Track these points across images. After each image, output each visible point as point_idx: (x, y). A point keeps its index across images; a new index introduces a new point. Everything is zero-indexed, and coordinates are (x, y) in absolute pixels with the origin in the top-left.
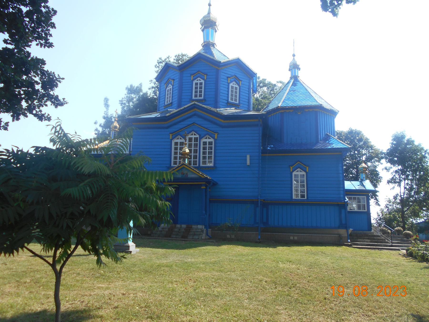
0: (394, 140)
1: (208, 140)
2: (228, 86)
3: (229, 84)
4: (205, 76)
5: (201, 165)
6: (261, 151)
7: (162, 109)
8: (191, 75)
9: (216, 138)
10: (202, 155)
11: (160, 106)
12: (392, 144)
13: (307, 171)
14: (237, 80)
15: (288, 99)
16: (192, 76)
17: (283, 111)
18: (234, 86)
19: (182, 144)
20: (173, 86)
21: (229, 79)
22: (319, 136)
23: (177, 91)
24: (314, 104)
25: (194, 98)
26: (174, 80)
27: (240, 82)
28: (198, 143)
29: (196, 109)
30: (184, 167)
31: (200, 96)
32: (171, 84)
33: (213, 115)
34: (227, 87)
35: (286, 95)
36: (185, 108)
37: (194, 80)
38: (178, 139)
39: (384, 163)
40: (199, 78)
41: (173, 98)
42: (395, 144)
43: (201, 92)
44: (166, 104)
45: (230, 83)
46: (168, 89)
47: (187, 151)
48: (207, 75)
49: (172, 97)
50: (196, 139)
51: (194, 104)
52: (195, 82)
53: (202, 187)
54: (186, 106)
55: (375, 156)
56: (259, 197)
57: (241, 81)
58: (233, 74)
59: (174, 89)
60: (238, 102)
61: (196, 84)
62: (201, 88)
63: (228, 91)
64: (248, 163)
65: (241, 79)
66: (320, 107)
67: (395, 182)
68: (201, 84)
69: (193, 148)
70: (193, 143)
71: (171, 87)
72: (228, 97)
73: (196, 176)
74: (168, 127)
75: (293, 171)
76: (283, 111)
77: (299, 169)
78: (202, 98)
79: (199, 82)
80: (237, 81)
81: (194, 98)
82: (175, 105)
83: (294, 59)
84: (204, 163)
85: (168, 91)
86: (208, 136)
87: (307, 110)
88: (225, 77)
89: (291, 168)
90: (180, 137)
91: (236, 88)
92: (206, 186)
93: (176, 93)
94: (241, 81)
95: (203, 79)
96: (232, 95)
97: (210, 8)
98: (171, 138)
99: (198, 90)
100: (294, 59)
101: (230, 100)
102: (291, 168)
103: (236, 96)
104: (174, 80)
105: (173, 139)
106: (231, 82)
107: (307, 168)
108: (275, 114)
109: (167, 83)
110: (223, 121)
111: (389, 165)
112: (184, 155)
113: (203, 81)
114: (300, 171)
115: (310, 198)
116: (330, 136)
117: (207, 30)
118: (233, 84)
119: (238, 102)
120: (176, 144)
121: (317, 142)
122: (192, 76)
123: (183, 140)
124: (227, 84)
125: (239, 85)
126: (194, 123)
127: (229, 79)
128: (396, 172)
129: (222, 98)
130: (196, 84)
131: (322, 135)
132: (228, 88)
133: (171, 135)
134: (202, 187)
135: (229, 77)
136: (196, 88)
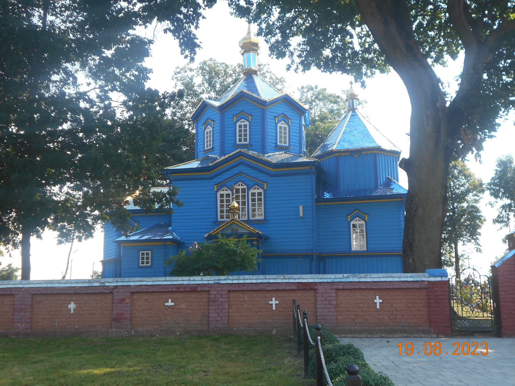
0: (499, 165)
1: (256, 191)
2: (276, 127)
3: (276, 124)
4: (250, 117)
5: (251, 218)
6: (314, 201)
7: (201, 155)
8: (234, 116)
9: (265, 188)
10: (250, 207)
11: (198, 151)
12: (496, 171)
13: (367, 220)
14: (286, 118)
15: (343, 140)
16: (235, 117)
17: (338, 154)
18: (283, 126)
19: (228, 195)
20: (213, 128)
21: (277, 118)
22: (379, 181)
23: (218, 134)
24: (371, 145)
25: (238, 142)
26: (214, 121)
27: (290, 121)
28: (246, 194)
29: (241, 157)
30: (234, 223)
31: (245, 140)
32: (211, 126)
33: (261, 163)
34: (274, 128)
35: (341, 134)
36: (229, 157)
37: (237, 121)
38: (255, 189)
39: (486, 197)
40: (243, 120)
41: (214, 142)
42: (500, 171)
43: (245, 135)
44: (206, 149)
45: (278, 123)
46: (207, 130)
47: (236, 205)
48: (251, 115)
49: (213, 141)
50: (243, 191)
51: (240, 152)
52: (238, 124)
53: (254, 243)
54: (231, 154)
55: (478, 188)
56: (314, 251)
57: (290, 119)
58: (281, 112)
59: (215, 132)
60: (287, 145)
61: (240, 126)
62: (245, 131)
63: (276, 133)
64: (301, 214)
65: (289, 117)
66: (379, 149)
67: (502, 222)
68: (245, 126)
69: (241, 200)
70: (240, 194)
71: (211, 129)
72: (276, 140)
73: (247, 231)
74: (211, 178)
75: (351, 220)
76: (338, 154)
77: (357, 218)
78: (248, 142)
79: (243, 124)
80: (285, 119)
81: (238, 142)
82: (217, 150)
83: (351, 87)
84: (254, 216)
85: (207, 134)
86: (257, 187)
87: (364, 153)
88: (272, 117)
89: (349, 217)
90: (225, 188)
91: (285, 128)
92: (258, 241)
93: (217, 136)
94: (290, 119)
95: (248, 121)
96: (281, 137)
97: (249, 26)
98: (216, 190)
99: (243, 133)
100: (351, 87)
101: (278, 143)
102: (349, 217)
103: (285, 138)
104: (214, 121)
105: (218, 190)
106: (279, 121)
107: (366, 216)
108: (330, 157)
109: (206, 124)
110: (272, 169)
111: (492, 199)
112: (232, 210)
113: (247, 123)
114: (359, 220)
115: (369, 249)
116: (391, 180)
117: (248, 54)
118: (282, 124)
119: (287, 145)
120: (222, 196)
121: (377, 188)
122: (235, 117)
123: (229, 192)
124: (274, 124)
125: (288, 124)
126: (240, 172)
127: (277, 118)
128: (504, 207)
129: (270, 141)
130: (240, 126)
131: (382, 180)
132: (276, 130)
133: (216, 186)
134: (254, 243)
135: (277, 117)
136: (240, 131)
